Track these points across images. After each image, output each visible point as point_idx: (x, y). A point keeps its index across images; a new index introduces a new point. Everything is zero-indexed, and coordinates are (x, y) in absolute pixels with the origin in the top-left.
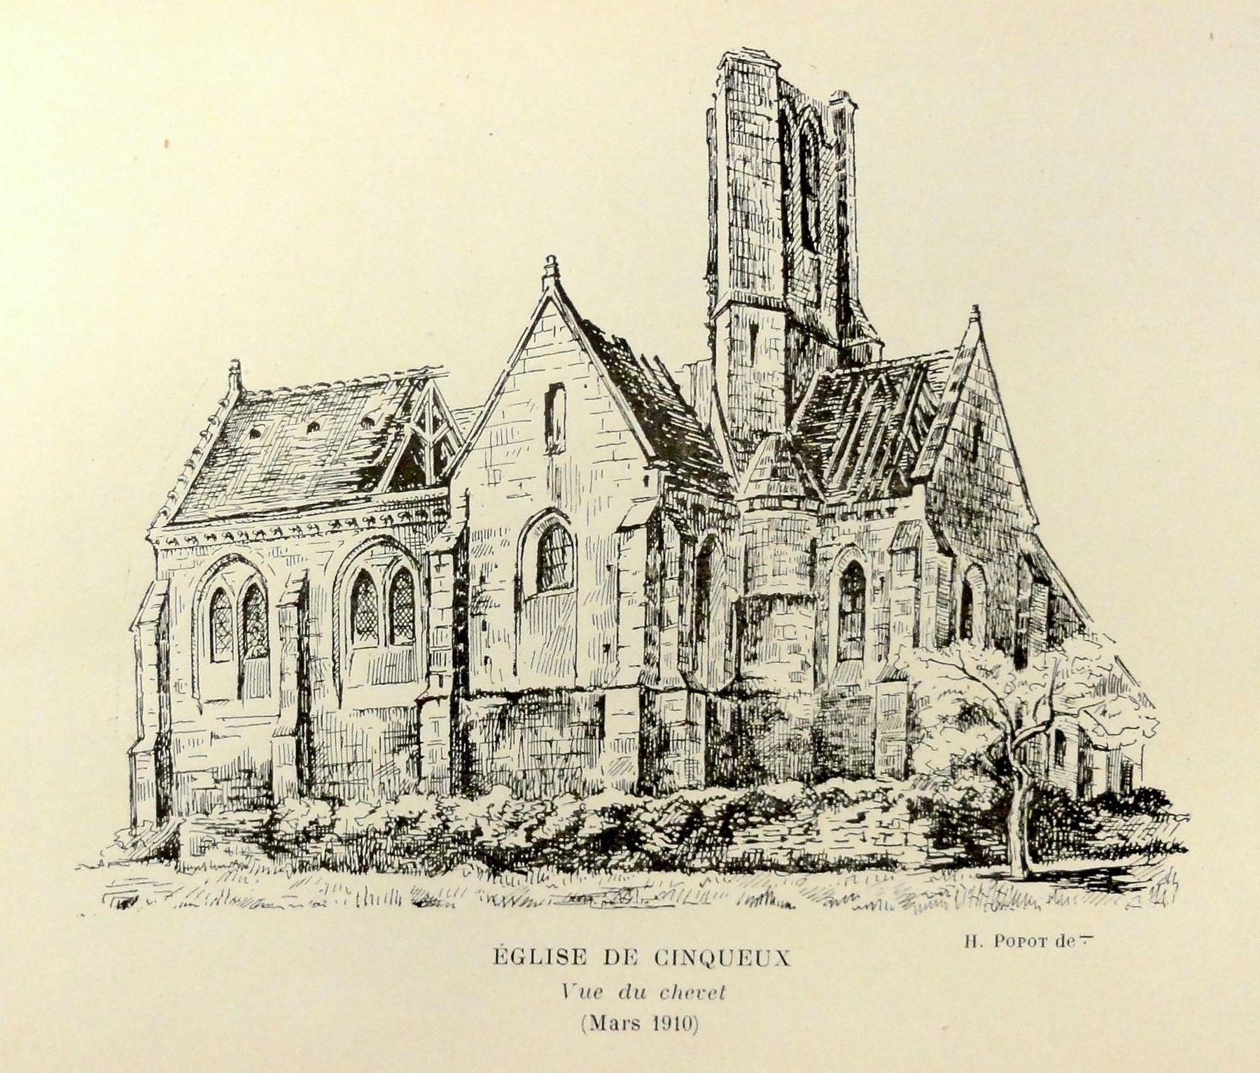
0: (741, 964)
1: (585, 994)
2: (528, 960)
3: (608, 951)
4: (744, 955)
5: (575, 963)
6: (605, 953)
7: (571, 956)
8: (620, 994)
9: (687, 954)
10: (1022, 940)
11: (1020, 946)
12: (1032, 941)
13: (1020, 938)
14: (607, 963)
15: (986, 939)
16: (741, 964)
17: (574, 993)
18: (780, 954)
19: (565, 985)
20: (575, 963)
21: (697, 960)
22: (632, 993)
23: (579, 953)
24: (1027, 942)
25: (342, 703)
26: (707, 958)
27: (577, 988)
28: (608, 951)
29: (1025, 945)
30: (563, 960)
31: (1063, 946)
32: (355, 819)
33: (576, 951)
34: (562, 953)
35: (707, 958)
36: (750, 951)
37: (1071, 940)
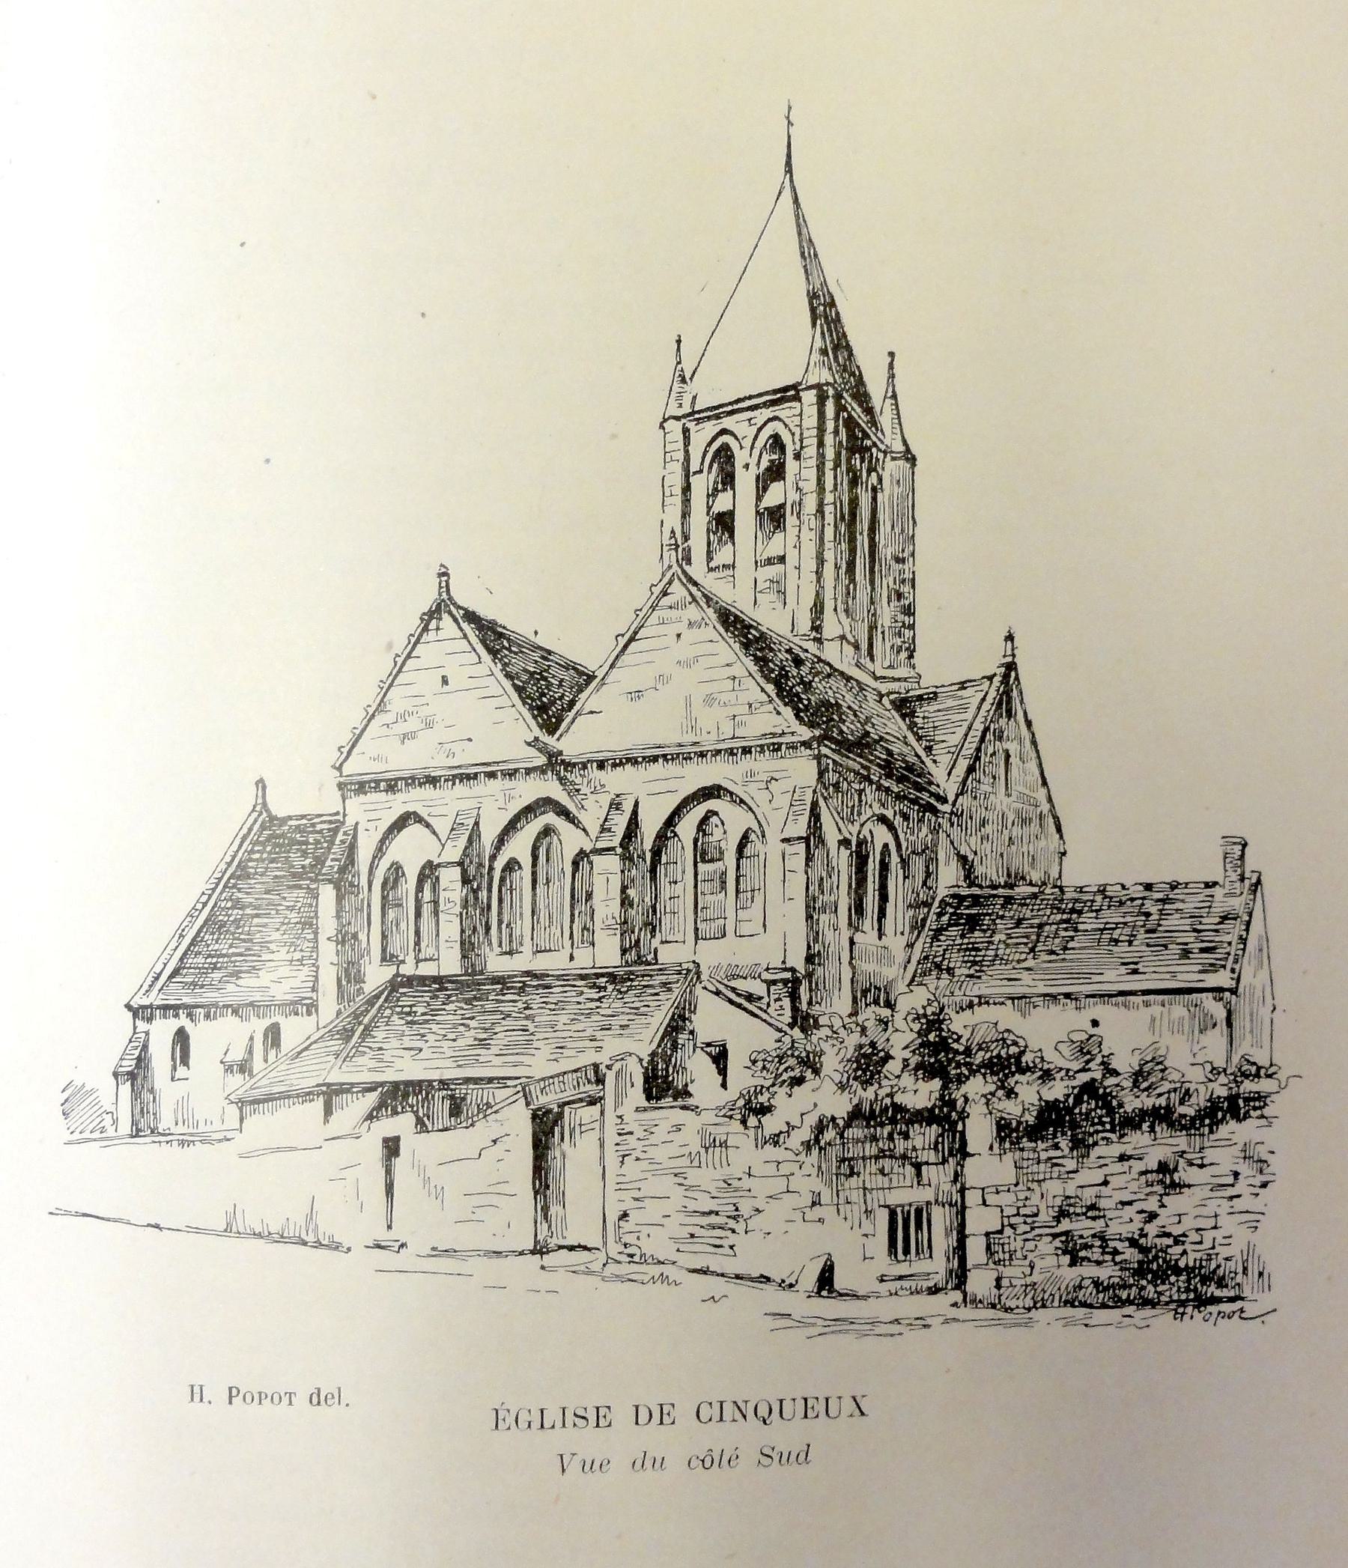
0: (806, 1416)
1: (587, 1468)
2: (536, 1424)
3: (637, 1407)
4: (601, 1414)
5: (598, 1425)
6: (540, 1412)
7: (592, 1416)
8: (609, 1462)
9: (739, 1408)
10: (263, 1396)
11: (260, 1403)
12: (276, 1397)
13: (260, 1393)
14: (637, 1423)
15: (216, 1392)
16: (806, 1416)
17: (574, 1468)
18: (855, 1400)
19: (561, 1456)
20: (598, 1425)
21: (750, 1413)
22: (648, 1463)
23: (602, 1412)
24: (269, 1398)
25: (1202, 1227)
26: (763, 1411)
27: (577, 1459)
28: (637, 1407)
29: (266, 1402)
30: (580, 1422)
31: (319, 1403)
32: (735, 1255)
33: (806, 1400)
34: (583, 1414)
35: (763, 1411)
36: (817, 1398)
37: (329, 1396)
